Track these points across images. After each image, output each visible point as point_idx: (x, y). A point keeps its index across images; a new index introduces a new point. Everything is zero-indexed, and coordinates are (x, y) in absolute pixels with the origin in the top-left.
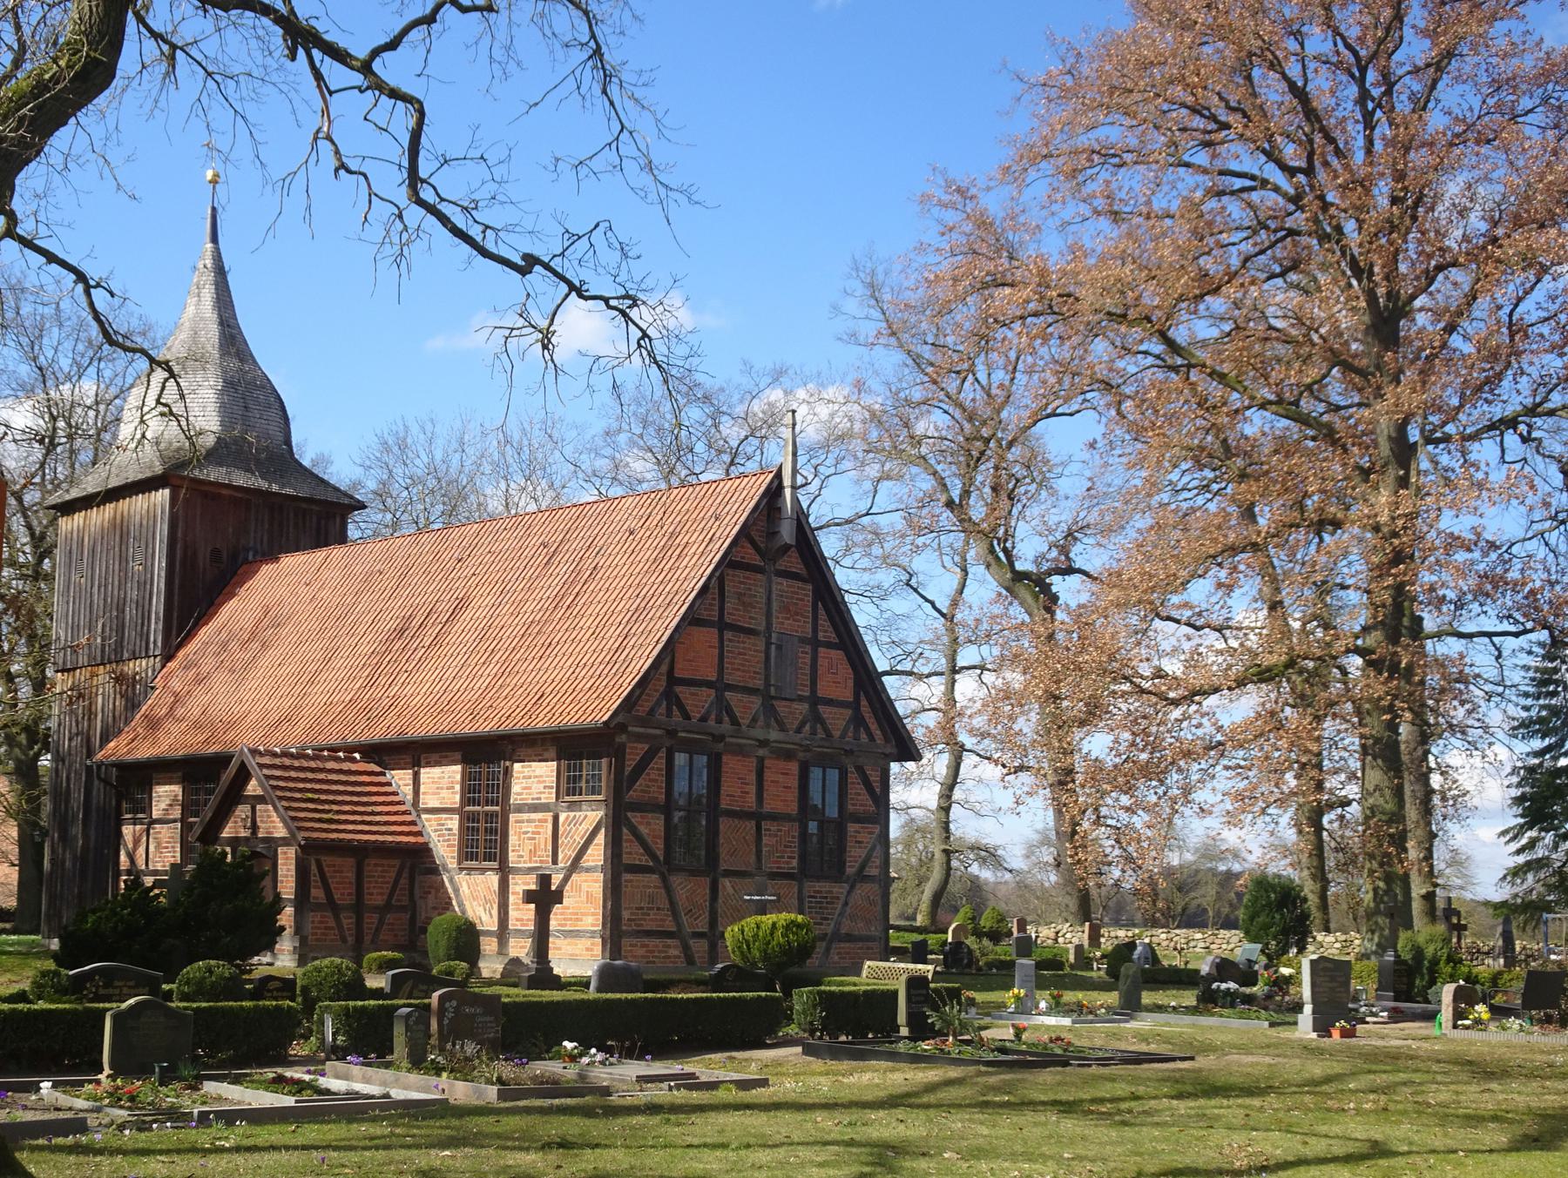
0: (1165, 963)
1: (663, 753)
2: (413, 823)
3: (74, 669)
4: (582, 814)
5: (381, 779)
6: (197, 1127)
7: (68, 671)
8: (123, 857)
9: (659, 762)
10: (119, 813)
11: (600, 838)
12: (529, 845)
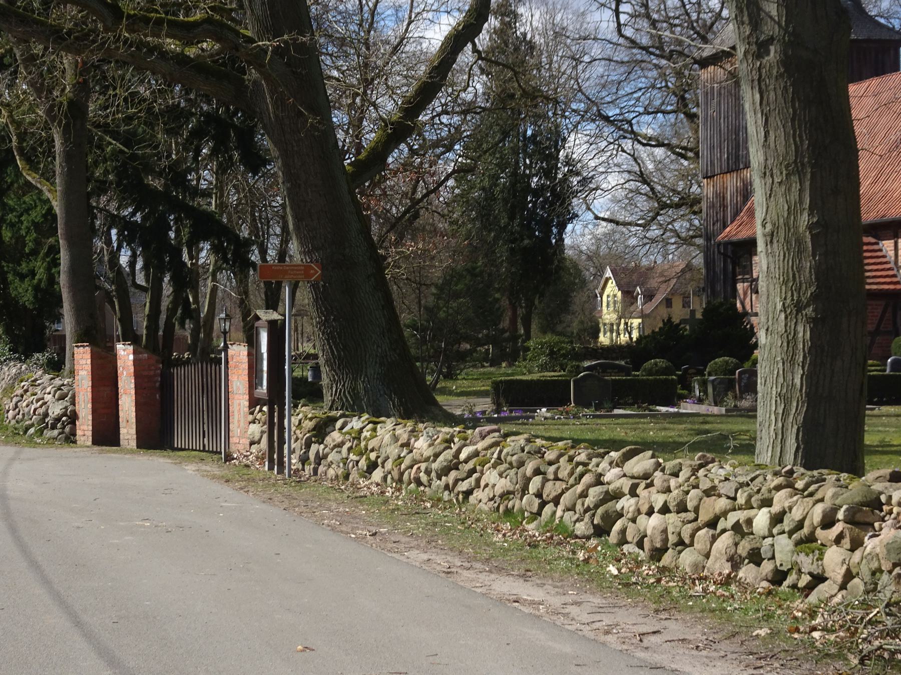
0: (131, 348)
2: (894, 276)
3: (714, 176)
5: (876, 247)
6: (731, 453)
7: (710, 177)
8: (739, 305)
10: (734, 275)
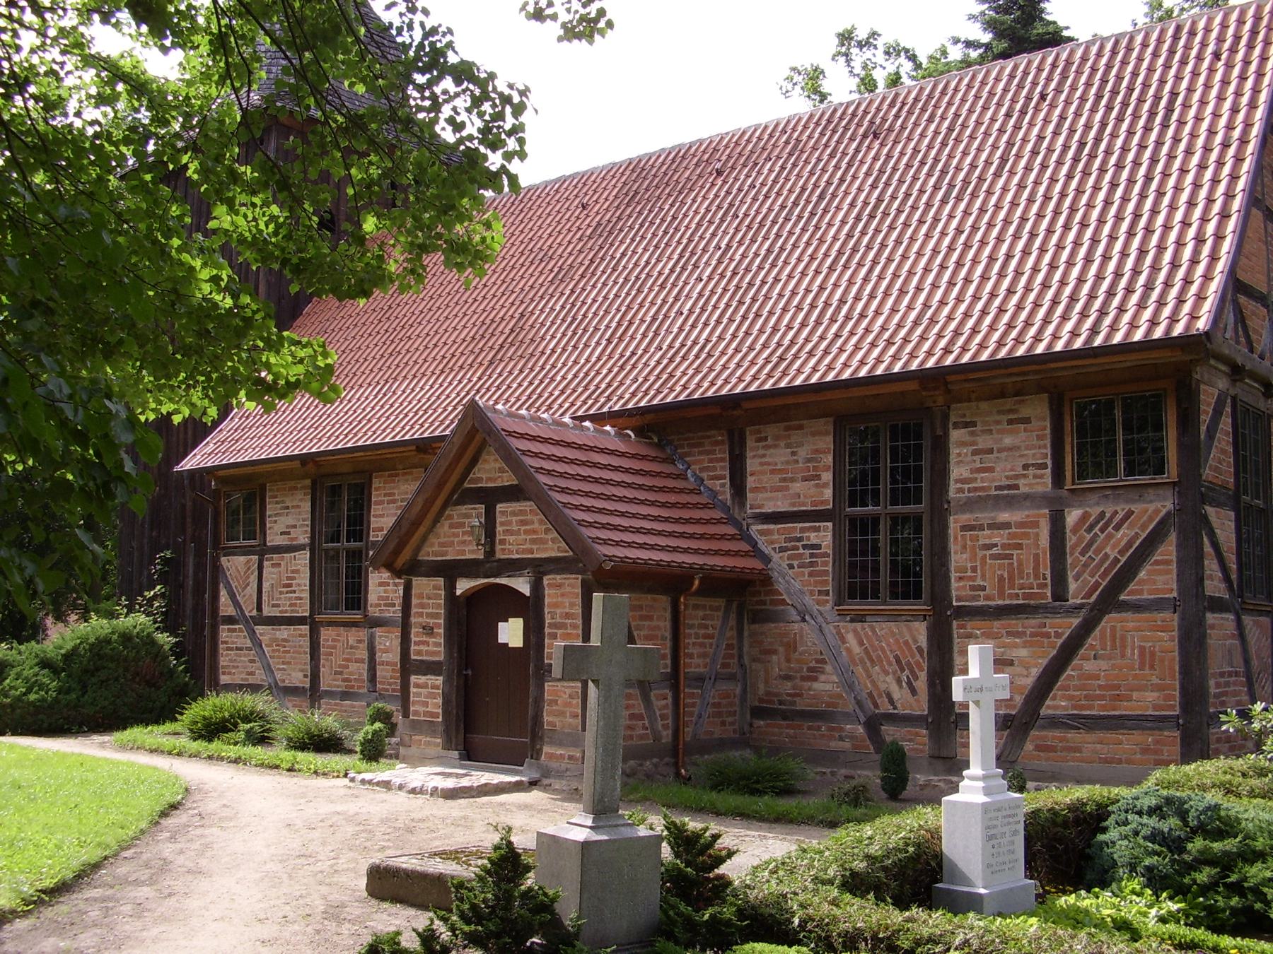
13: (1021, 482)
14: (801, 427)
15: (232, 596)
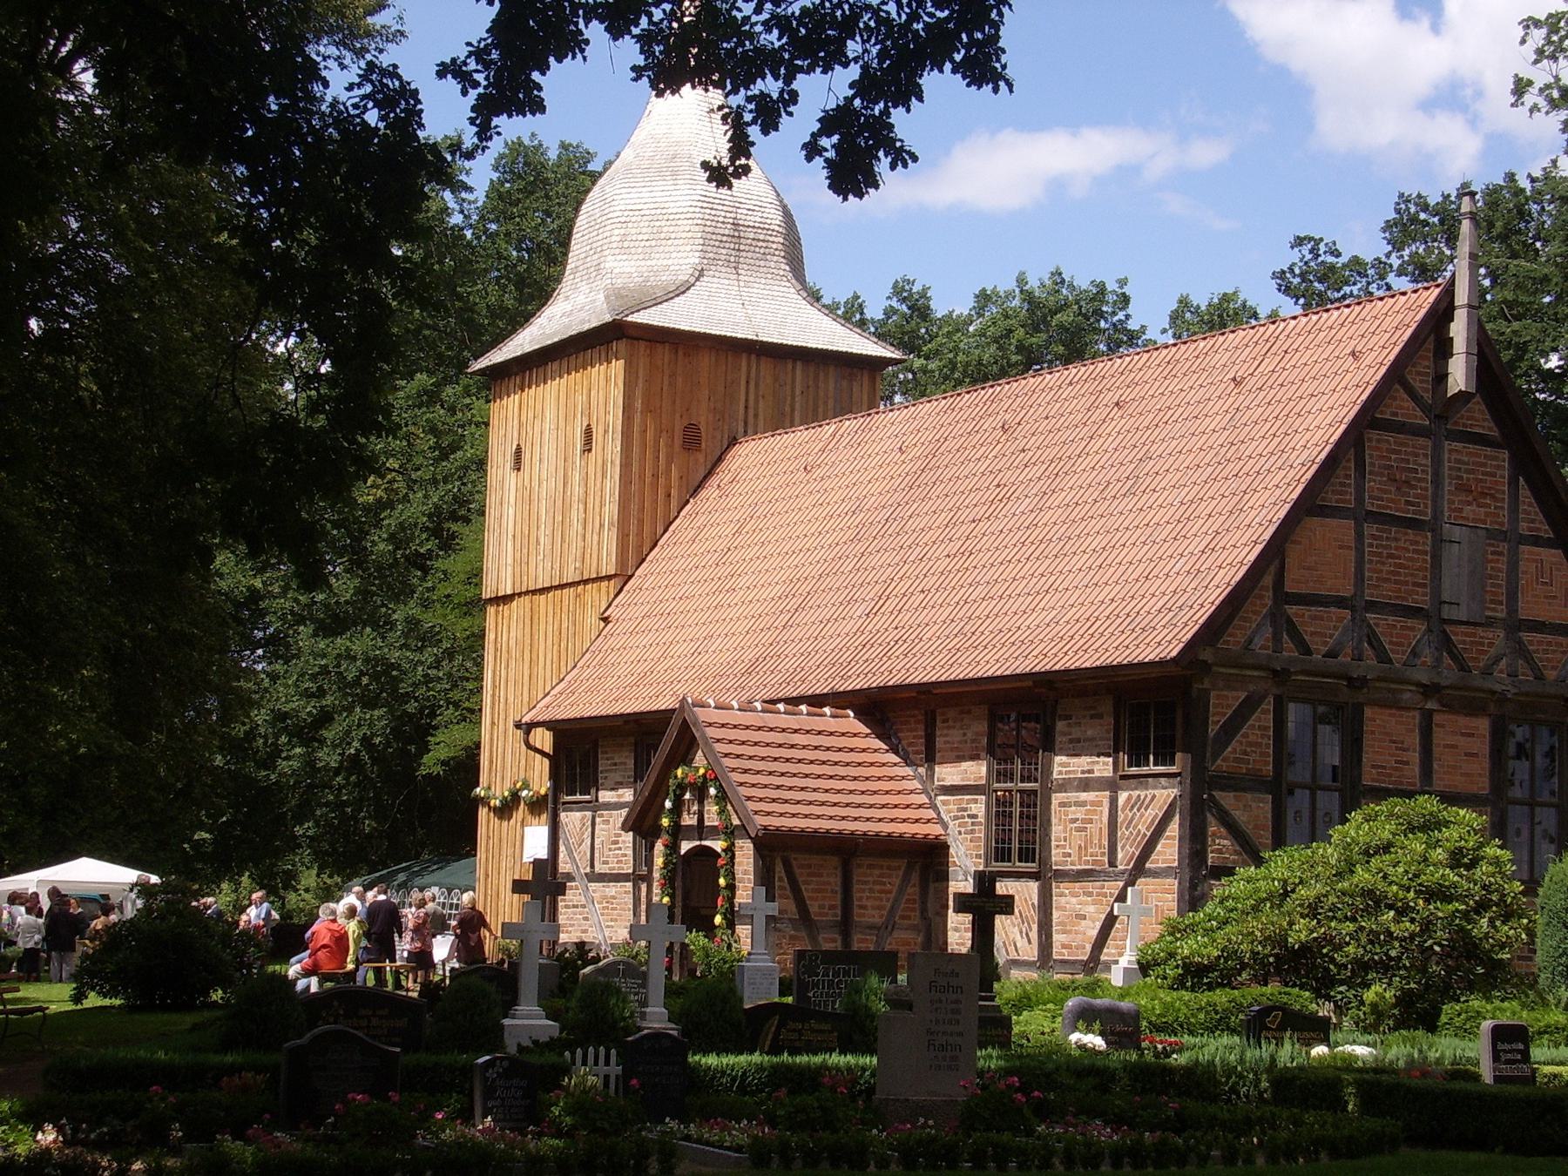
1: (1269, 704)
4: (1150, 792)
9: (1264, 717)
11: (1174, 828)
12: (1078, 839)
13: (1096, 768)
14: (969, 712)
15: (570, 853)
